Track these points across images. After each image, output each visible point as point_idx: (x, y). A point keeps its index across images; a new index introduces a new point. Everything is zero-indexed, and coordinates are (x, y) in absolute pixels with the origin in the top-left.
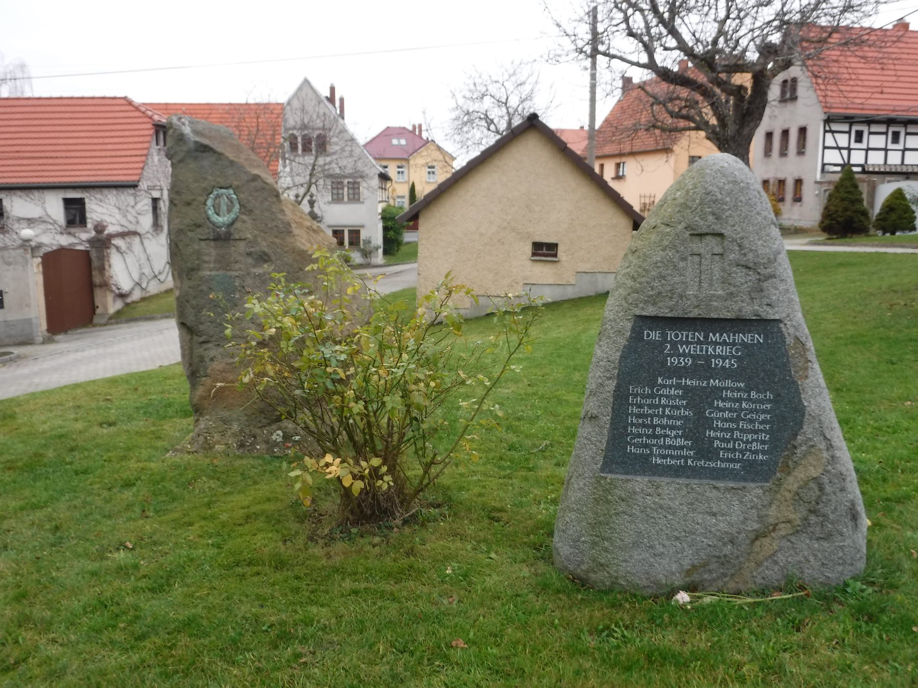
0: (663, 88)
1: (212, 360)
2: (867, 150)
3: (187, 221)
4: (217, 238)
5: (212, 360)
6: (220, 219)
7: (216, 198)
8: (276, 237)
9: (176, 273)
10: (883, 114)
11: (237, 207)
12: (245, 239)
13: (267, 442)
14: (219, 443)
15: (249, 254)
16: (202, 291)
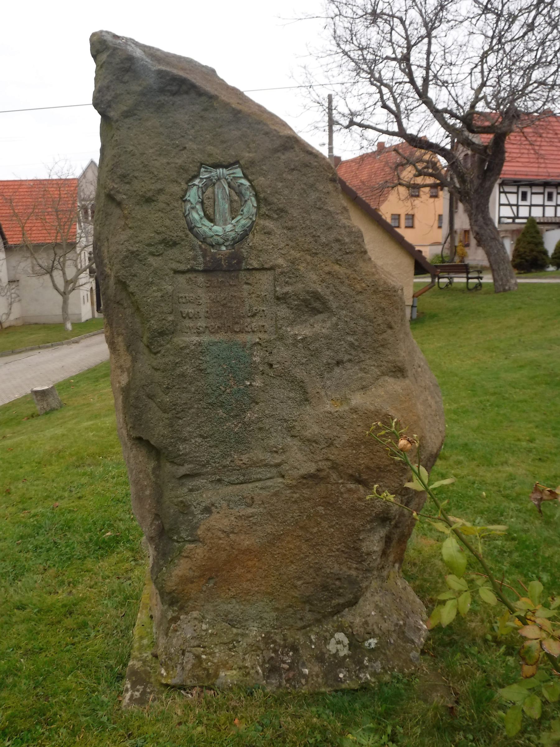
0: (409, 150)
1: (207, 510)
2: (531, 206)
3: (147, 235)
4: (212, 269)
5: (207, 510)
7: (206, 186)
8: (337, 262)
9: (120, 340)
10: (542, 179)
11: (251, 204)
12: (272, 268)
13: (320, 658)
14: (225, 665)
15: (281, 299)
16: (183, 375)
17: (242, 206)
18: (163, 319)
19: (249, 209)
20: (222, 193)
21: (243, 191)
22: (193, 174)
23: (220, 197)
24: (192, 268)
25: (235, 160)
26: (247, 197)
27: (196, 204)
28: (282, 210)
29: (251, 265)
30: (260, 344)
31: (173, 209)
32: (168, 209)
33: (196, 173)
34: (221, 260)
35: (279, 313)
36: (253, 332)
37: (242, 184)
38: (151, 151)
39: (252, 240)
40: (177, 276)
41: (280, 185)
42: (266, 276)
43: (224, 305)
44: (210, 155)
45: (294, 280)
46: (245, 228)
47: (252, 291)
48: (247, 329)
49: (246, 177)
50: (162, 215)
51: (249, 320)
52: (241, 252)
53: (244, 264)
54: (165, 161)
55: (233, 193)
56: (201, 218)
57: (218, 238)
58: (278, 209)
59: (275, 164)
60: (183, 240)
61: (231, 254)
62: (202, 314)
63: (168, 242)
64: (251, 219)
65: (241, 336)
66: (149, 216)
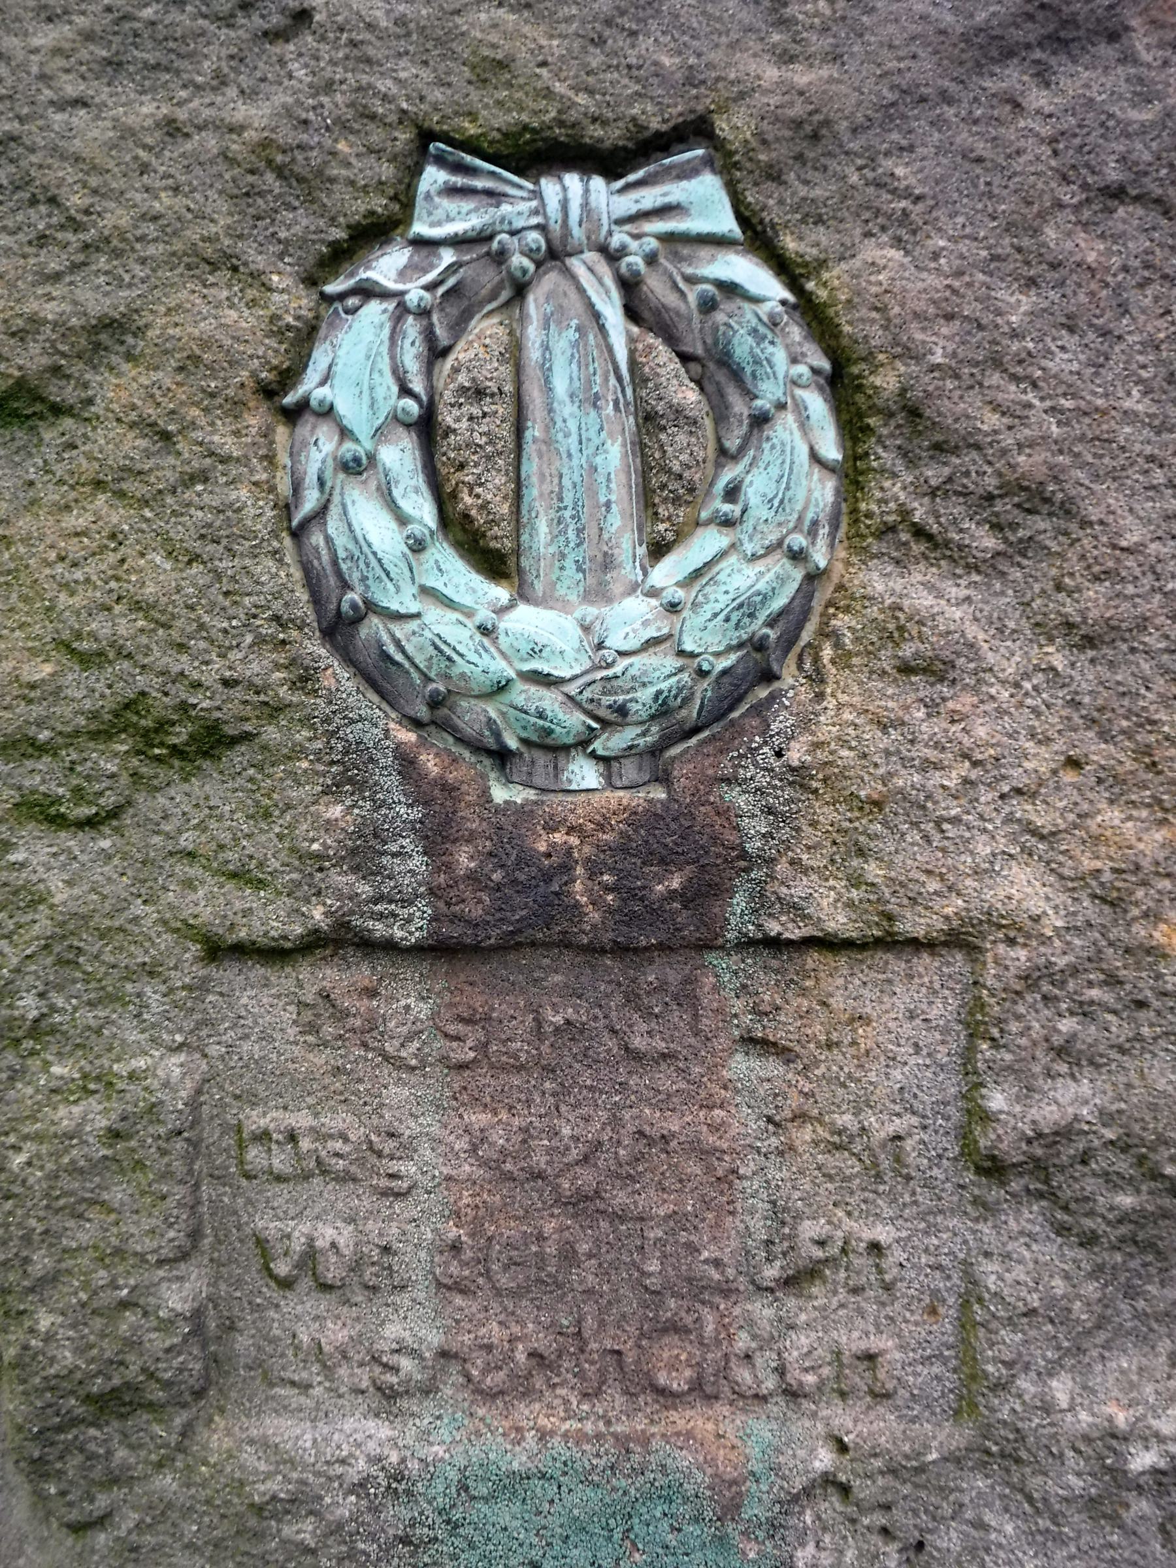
4: (504, 927)
6: (548, 630)
7: (459, 301)
11: (794, 458)
12: (960, 940)
17: (724, 455)
18: (124, 1305)
19: (786, 480)
20: (571, 360)
21: (742, 347)
22: (358, 208)
23: (561, 385)
24: (342, 925)
25: (677, 110)
26: (769, 392)
27: (379, 433)
28: (1034, 497)
29: (796, 910)
30: (845, 1490)
31: (203, 477)
32: (167, 469)
33: (379, 203)
34: (566, 868)
35: (990, 1273)
36: (793, 1394)
37: (730, 289)
38: (45, 37)
39: (806, 723)
40: (228, 974)
41: (1019, 305)
42: (904, 997)
43: (582, 1204)
44: (493, 69)
45: (1119, 1029)
46: (756, 626)
47: (794, 1101)
48: (744, 1375)
49: (758, 238)
50: (118, 517)
51: (763, 1311)
52: (723, 811)
53: (739, 902)
54: (148, 109)
55: (663, 356)
56: (418, 546)
57: (549, 701)
58: (1008, 489)
59: (981, 148)
60: (274, 711)
61: (647, 820)
62: (415, 1262)
63: (163, 726)
64: (797, 556)
65: (696, 1419)
66: (24, 523)
